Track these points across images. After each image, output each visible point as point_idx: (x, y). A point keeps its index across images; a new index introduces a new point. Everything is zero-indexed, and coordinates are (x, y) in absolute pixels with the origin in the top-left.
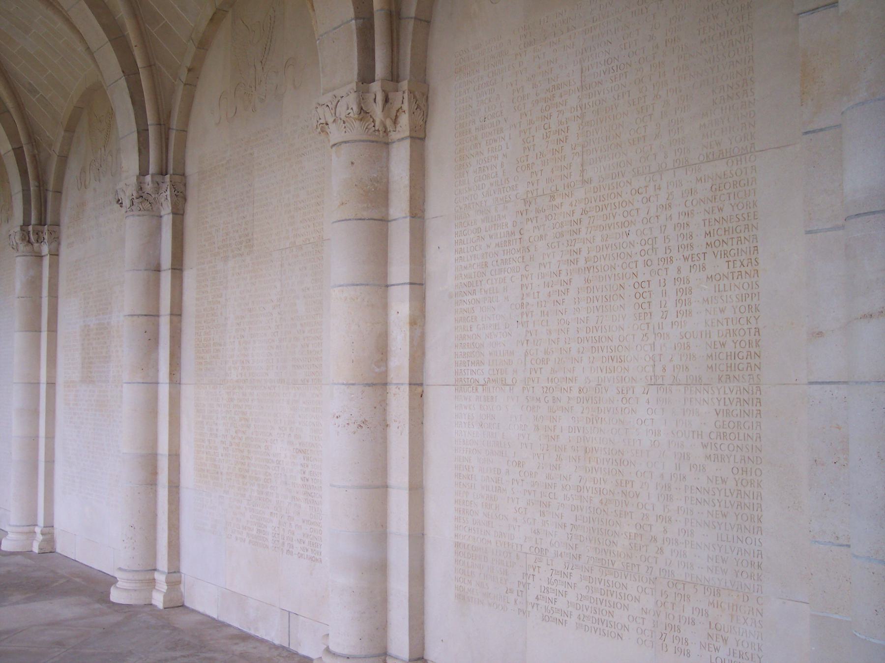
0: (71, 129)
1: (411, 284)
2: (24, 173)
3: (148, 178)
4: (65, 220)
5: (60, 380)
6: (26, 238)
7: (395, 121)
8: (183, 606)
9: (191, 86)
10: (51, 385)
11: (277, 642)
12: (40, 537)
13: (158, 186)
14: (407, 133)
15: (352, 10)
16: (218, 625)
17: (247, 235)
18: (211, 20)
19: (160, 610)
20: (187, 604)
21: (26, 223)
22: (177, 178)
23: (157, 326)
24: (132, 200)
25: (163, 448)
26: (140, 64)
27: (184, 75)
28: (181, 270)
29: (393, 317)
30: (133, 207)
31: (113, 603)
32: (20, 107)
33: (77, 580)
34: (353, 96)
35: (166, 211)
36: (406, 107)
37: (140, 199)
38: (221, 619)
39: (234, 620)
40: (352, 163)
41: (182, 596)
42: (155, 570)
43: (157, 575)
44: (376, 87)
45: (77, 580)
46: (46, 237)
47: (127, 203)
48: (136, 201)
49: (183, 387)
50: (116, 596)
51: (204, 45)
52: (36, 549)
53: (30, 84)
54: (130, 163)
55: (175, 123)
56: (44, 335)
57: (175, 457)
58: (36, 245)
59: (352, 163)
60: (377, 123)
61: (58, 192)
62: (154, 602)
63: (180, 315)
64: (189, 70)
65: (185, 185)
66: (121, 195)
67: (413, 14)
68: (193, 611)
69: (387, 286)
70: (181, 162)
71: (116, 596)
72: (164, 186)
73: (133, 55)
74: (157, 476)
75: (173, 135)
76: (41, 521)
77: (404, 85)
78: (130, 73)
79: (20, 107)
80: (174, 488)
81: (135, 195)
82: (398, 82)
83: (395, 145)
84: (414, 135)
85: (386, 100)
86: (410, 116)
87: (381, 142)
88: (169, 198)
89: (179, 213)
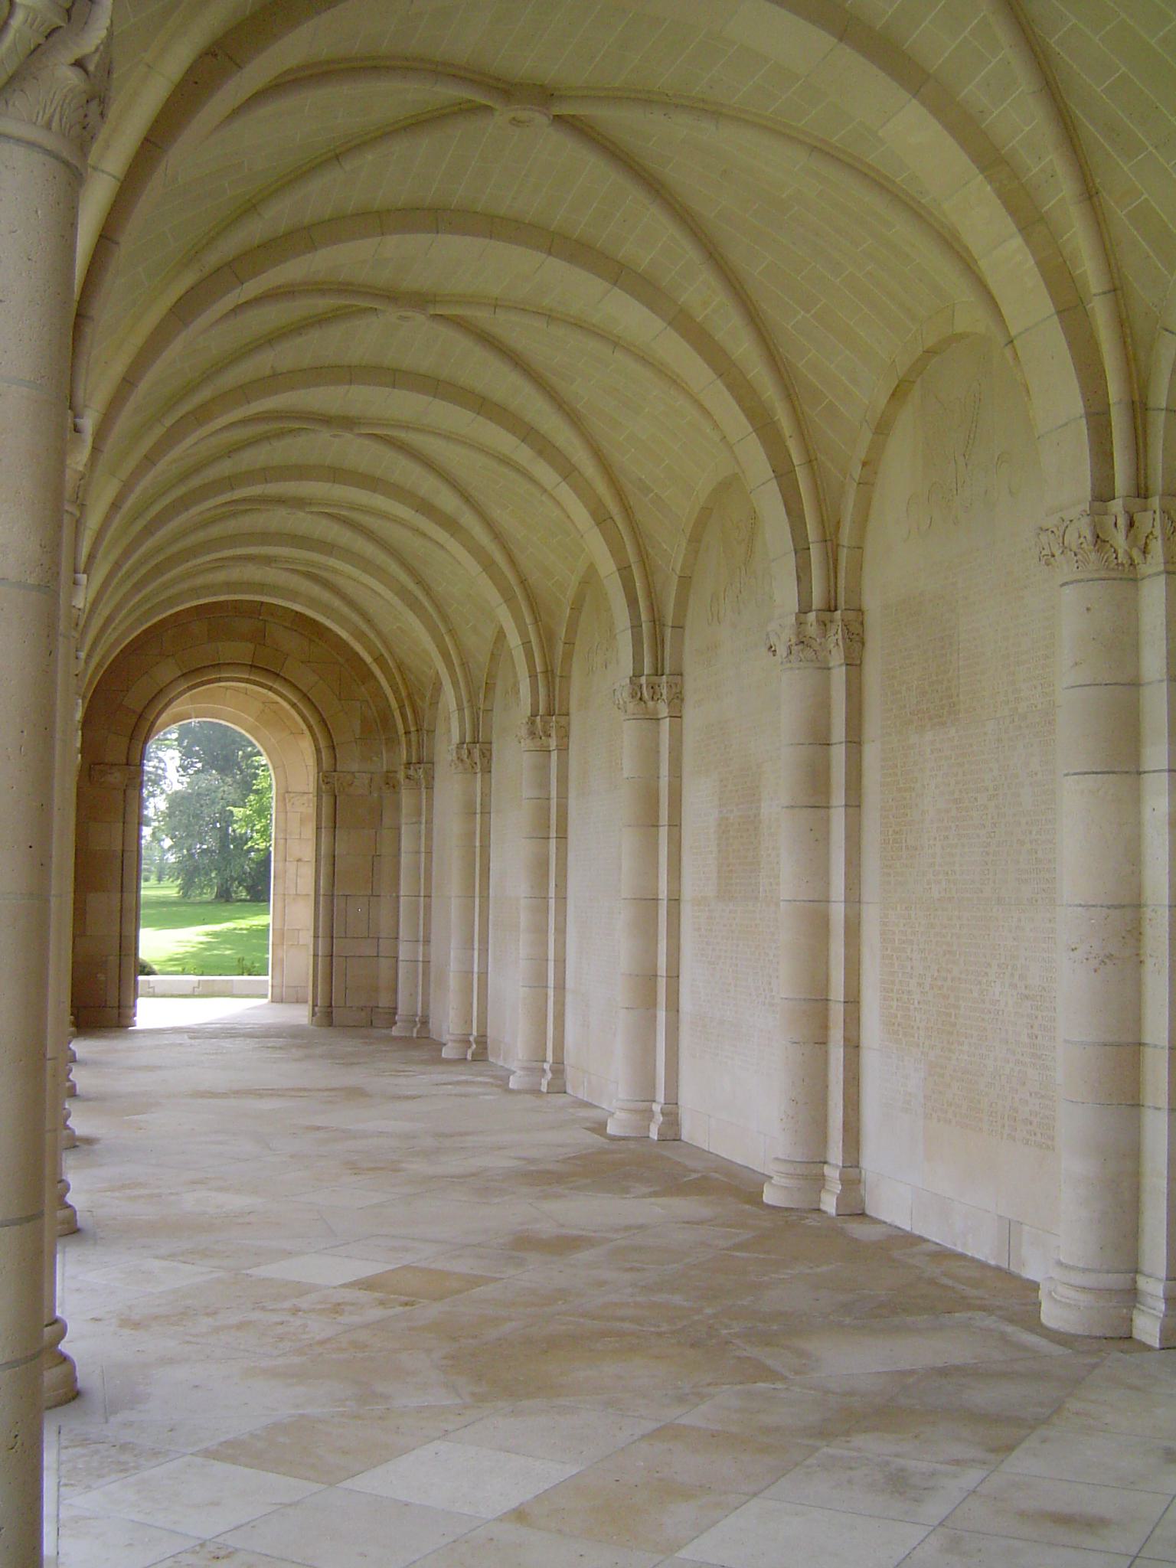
0: (696, 539)
1: (1170, 771)
2: (632, 602)
3: (812, 616)
4: (690, 668)
5: (688, 892)
6: (637, 695)
7: (1145, 552)
8: (862, 1215)
9: (866, 485)
10: (675, 901)
11: (992, 1262)
12: (660, 1118)
13: (823, 624)
14: (1162, 568)
15: (1081, 404)
16: (912, 1240)
17: (951, 697)
18: (893, 395)
19: (830, 1218)
20: (867, 1212)
21: (637, 674)
22: (851, 615)
23: (827, 821)
24: (790, 647)
25: (837, 992)
26: (796, 462)
27: (857, 472)
28: (859, 743)
29: (1147, 814)
30: (792, 657)
31: (768, 1206)
32: (627, 511)
33: (717, 1175)
34: (1086, 520)
35: (837, 658)
36: (1157, 532)
37: (801, 647)
38: (917, 1232)
39: (934, 1232)
40: (1088, 609)
41: (863, 1201)
42: (825, 1163)
43: (827, 1170)
44: (1117, 506)
45: (717, 1175)
46: (664, 692)
47: (782, 651)
48: (795, 648)
49: (864, 907)
50: (769, 1196)
51: (883, 428)
52: (654, 1135)
53: (640, 479)
54: (786, 596)
55: (846, 537)
56: (663, 832)
57: (853, 1002)
58: (651, 704)
59: (1088, 609)
60: (1120, 552)
61: (679, 627)
62: (823, 1207)
63: (859, 806)
64: (864, 464)
65: (862, 624)
66: (773, 640)
67: (1164, 405)
68: (875, 1221)
69: (1139, 773)
70: (856, 590)
71: (769, 1196)
72: (833, 628)
73: (787, 451)
74: (826, 1022)
75: (844, 555)
76: (661, 1097)
77: (1155, 502)
78: (784, 475)
79: (627, 511)
80: (853, 1046)
81: (793, 641)
82: (1146, 497)
83: (1146, 582)
84: (1171, 568)
85: (1131, 524)
86: (1164, 545)
87: (1129, 575)
88: (840, 643)
89: (854, 664)
